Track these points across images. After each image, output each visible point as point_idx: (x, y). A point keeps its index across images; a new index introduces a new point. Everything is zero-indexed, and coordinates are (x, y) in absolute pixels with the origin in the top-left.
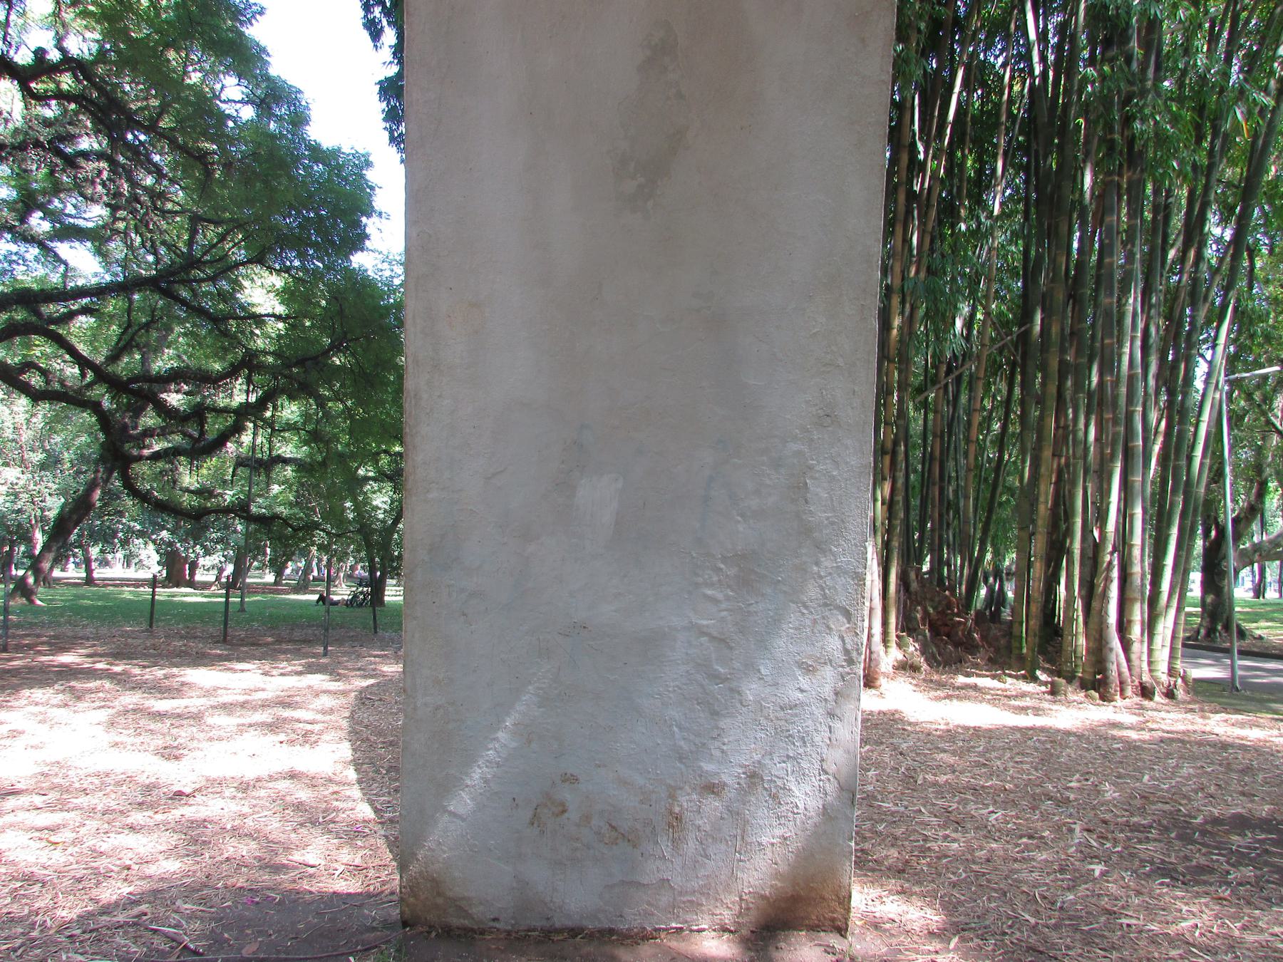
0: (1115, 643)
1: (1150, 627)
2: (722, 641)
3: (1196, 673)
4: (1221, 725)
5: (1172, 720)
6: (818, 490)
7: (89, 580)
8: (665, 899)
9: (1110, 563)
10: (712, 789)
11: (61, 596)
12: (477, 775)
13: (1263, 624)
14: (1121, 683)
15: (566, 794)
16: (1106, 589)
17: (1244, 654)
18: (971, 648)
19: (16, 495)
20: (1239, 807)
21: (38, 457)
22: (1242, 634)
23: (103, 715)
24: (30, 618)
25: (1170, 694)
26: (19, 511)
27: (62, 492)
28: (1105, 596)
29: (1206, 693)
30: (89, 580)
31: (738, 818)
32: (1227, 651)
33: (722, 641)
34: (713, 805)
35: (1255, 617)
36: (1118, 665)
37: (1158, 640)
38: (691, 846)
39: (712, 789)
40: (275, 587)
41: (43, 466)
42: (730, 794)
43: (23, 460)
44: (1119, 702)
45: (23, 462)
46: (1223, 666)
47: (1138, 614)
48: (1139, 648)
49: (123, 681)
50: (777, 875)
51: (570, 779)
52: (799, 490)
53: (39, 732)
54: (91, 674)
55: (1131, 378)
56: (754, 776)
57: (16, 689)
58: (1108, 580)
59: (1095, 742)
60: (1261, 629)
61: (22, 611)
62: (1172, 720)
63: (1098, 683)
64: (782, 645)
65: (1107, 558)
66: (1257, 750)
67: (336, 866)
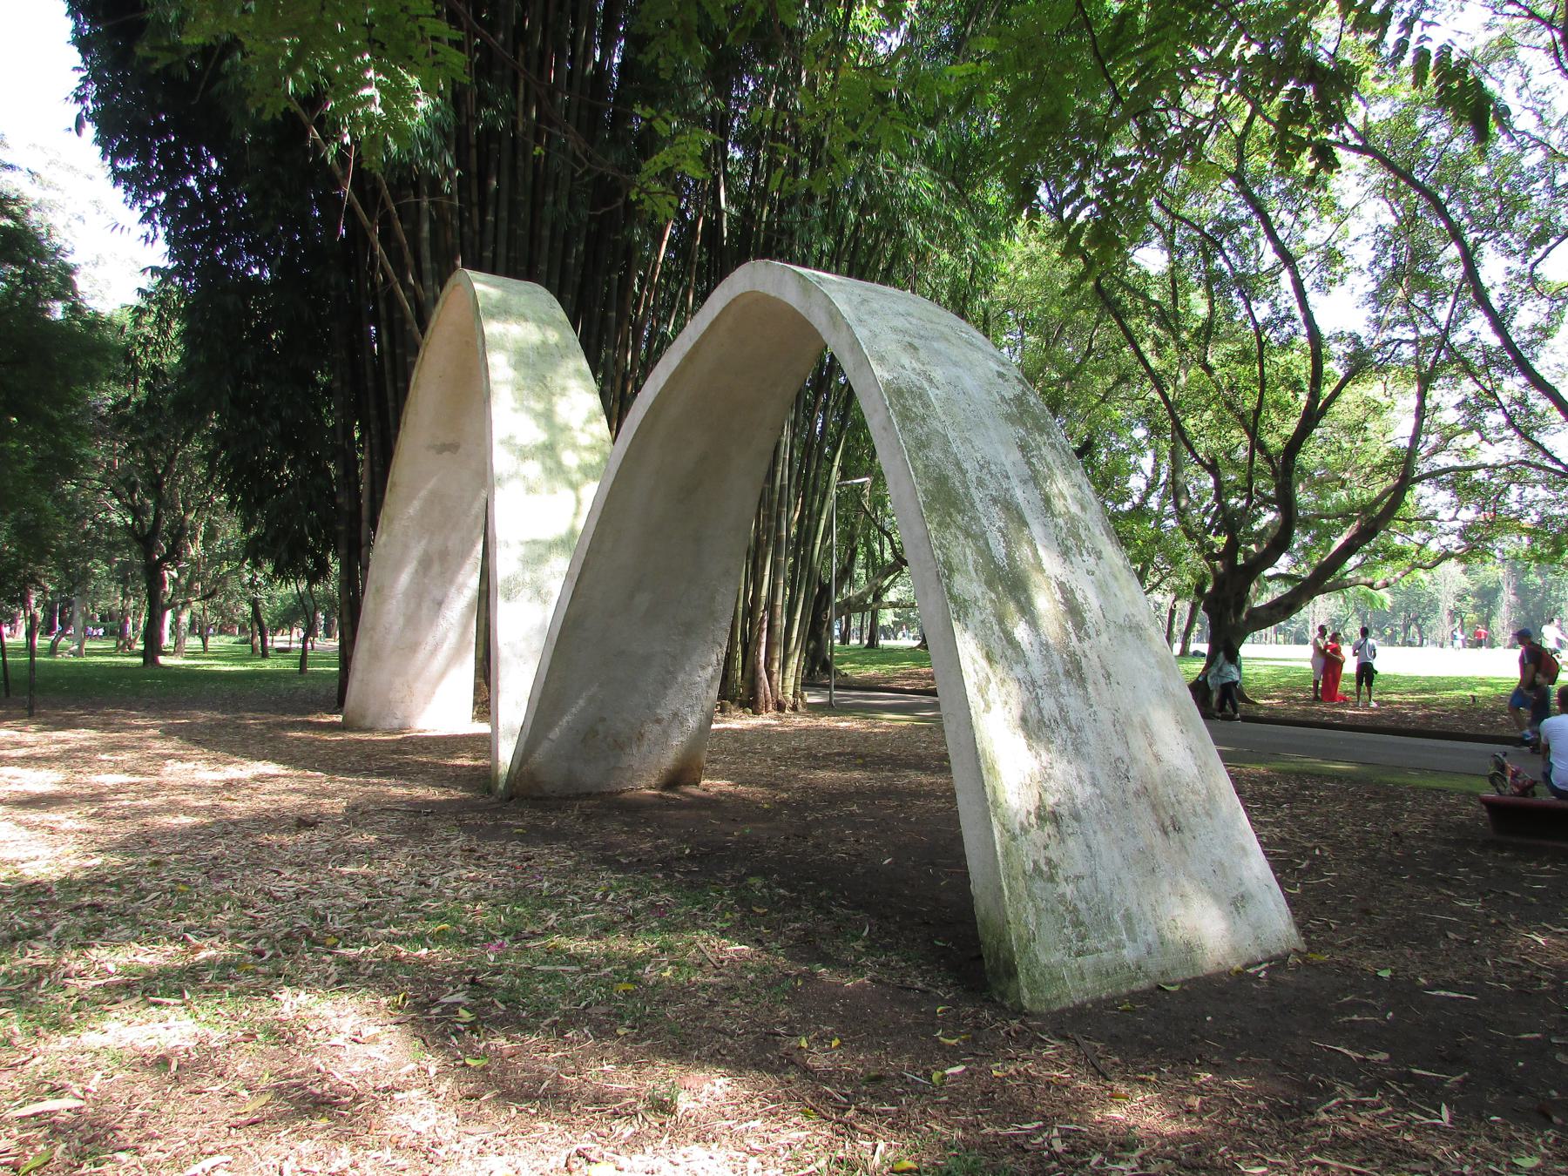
0: (764, 675)
1: (784, 665)
2: (674, 657)
3: (810, 700)
4: (825, 722)
5: (801, 721)
6: (719, 598)
8: (629, 774)
10: (659, 721)
12: (567, 718)
13: (848, 665)
15: (601, 728)
16: (760, 636)
17: (837, 687)
20: (840, 750)
22: (837, 672)
25: (794, 708)
28: (758, 643)
29: (814, 709)
31: (666, 734)
32: (827, 687)
33: (674, 657)
34: (657, 728)
35: (843, 660)
37: (789, 672)
38: (645, 748)
39: (659, 721)
40: (78, 654)
42: (665, 723)
46: (824, 696)
47: (778, 654)
48: (777, 677)
51: (603, 720)
52: (713, 599)
55: (782, 487)
56: (675, 715)
58: (761, 630)
59: (763, 734)
60: (847, 669)
62: (801, 721)
64: (695, 658)
66: (846, 731)
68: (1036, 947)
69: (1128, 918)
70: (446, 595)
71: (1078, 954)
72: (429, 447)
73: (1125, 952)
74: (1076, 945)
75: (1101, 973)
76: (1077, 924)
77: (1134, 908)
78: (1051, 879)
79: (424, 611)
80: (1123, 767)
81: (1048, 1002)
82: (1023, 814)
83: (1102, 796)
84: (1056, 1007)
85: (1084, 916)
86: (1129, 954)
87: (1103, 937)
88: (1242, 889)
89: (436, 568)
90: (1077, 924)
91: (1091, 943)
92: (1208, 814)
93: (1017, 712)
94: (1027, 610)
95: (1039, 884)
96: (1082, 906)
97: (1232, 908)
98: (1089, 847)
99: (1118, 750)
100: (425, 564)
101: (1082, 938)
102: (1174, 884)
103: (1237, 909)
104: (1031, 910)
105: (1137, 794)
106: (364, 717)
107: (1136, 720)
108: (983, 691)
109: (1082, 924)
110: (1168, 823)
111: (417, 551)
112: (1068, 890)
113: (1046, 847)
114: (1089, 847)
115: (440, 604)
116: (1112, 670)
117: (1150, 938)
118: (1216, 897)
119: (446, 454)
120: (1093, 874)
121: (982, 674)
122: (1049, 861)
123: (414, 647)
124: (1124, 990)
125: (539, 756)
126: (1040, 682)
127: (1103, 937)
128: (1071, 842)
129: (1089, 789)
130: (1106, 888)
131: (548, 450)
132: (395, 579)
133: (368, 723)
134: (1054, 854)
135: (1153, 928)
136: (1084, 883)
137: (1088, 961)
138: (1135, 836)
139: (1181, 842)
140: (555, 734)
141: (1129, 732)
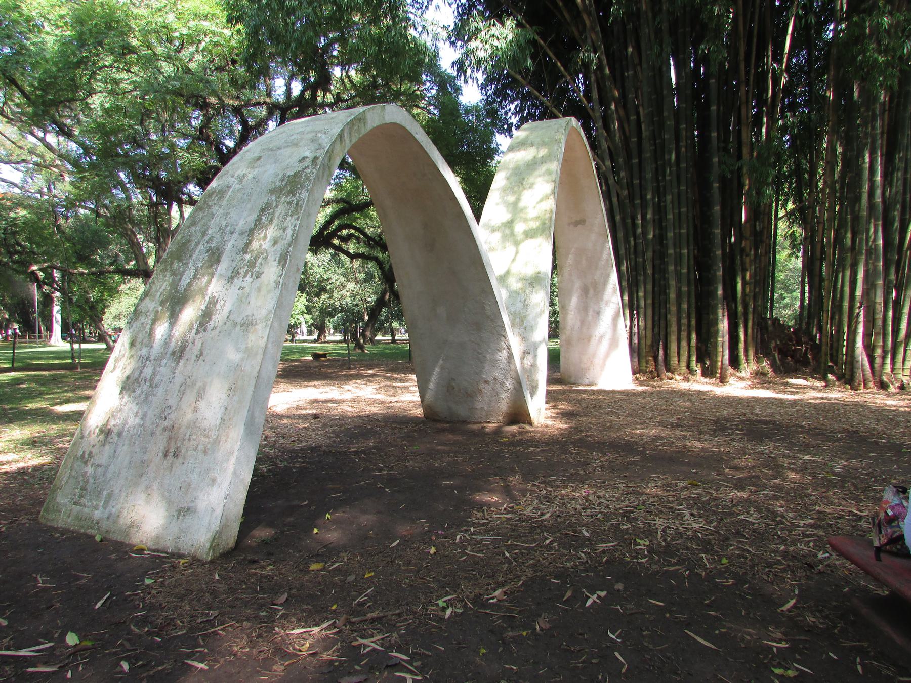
7: (394, 341)
9: (858, 313)
11: (376, 349)
14: (864, 380)
18: (806, 363)
19: (354, 296)
21: (362, 276)
23: (377, 386)
24: (362, 358)
26: (357, 305)
27: (375, 293)
30: (394, 341)
36: (863, 371)
41: (365, 281)
43: (356, 278)
44: (862, 390)
45: (356, 280)
49: (388, 379)
50: (509, 407)
53: (354, 390)
54: (378, 376)
57: (351, 380)
61: (359, 355)
63: (848, 379)
65: (857, 310)
67: (418, 412)
68: (59, 492)
69: (110, 495)
70: (600, 307)
71: (74, 504)
72: (569, 224)
73: (96, 512)
74: (77, 498)
75: (78, 518)
76: (84, 488)
77: (117, 491)
78: (86, 463)
79: (590, 318)
80: (168, 411)
81: (48, 520)
82: (94, 426)
83: (143, 425)
84: (49, 524)
85: (89, 487)
86: (97, 514)
87: (91, 500)
88: (193, 505)
89: (591, 292)
90: (84, 488)
91: (83, 500)
92: (205, 452)
93: (127, 373)
94: (174, 317)
95: (79, 463)
96: (91, 481)
97: (176, 514)
98: (115, 452)
99: (172, 402)
100: (585, 291)
101: (81, 496)
102: (148, 487)
103: (179, 515)
104: (67, 475)
105: (164, 429)
106: (570, 377)
107: (199, 384)
108: (117, 360)
109: (86, 490)
110: (172, 450)
111: (578, 285)
112: (90, 470)
113: (93, 446)
114: (115, 452)
115: (598, 313)
116: (205, 353)
117: (114, 510)
118: (169, 503)
119: (580, 226)
120: (107, 467)
121: (123, 352)
122: (91, 453)
123: (589, 339)
124: (82, 531)
125: (429, 396)
126: (152, 358)
127: (91, 500)
128: (107, 447)
129: (138, 421)
130: (109, 475)
131: (510, 224)
132: (570, 300)
133: (573, 380)
134: (94, 451)
135: (119, 506)
136: (100, 470)
137: (78, 508)
138: (144, 453)
139: (172, 464)
140: (432, 386)
141: (188, 392)
